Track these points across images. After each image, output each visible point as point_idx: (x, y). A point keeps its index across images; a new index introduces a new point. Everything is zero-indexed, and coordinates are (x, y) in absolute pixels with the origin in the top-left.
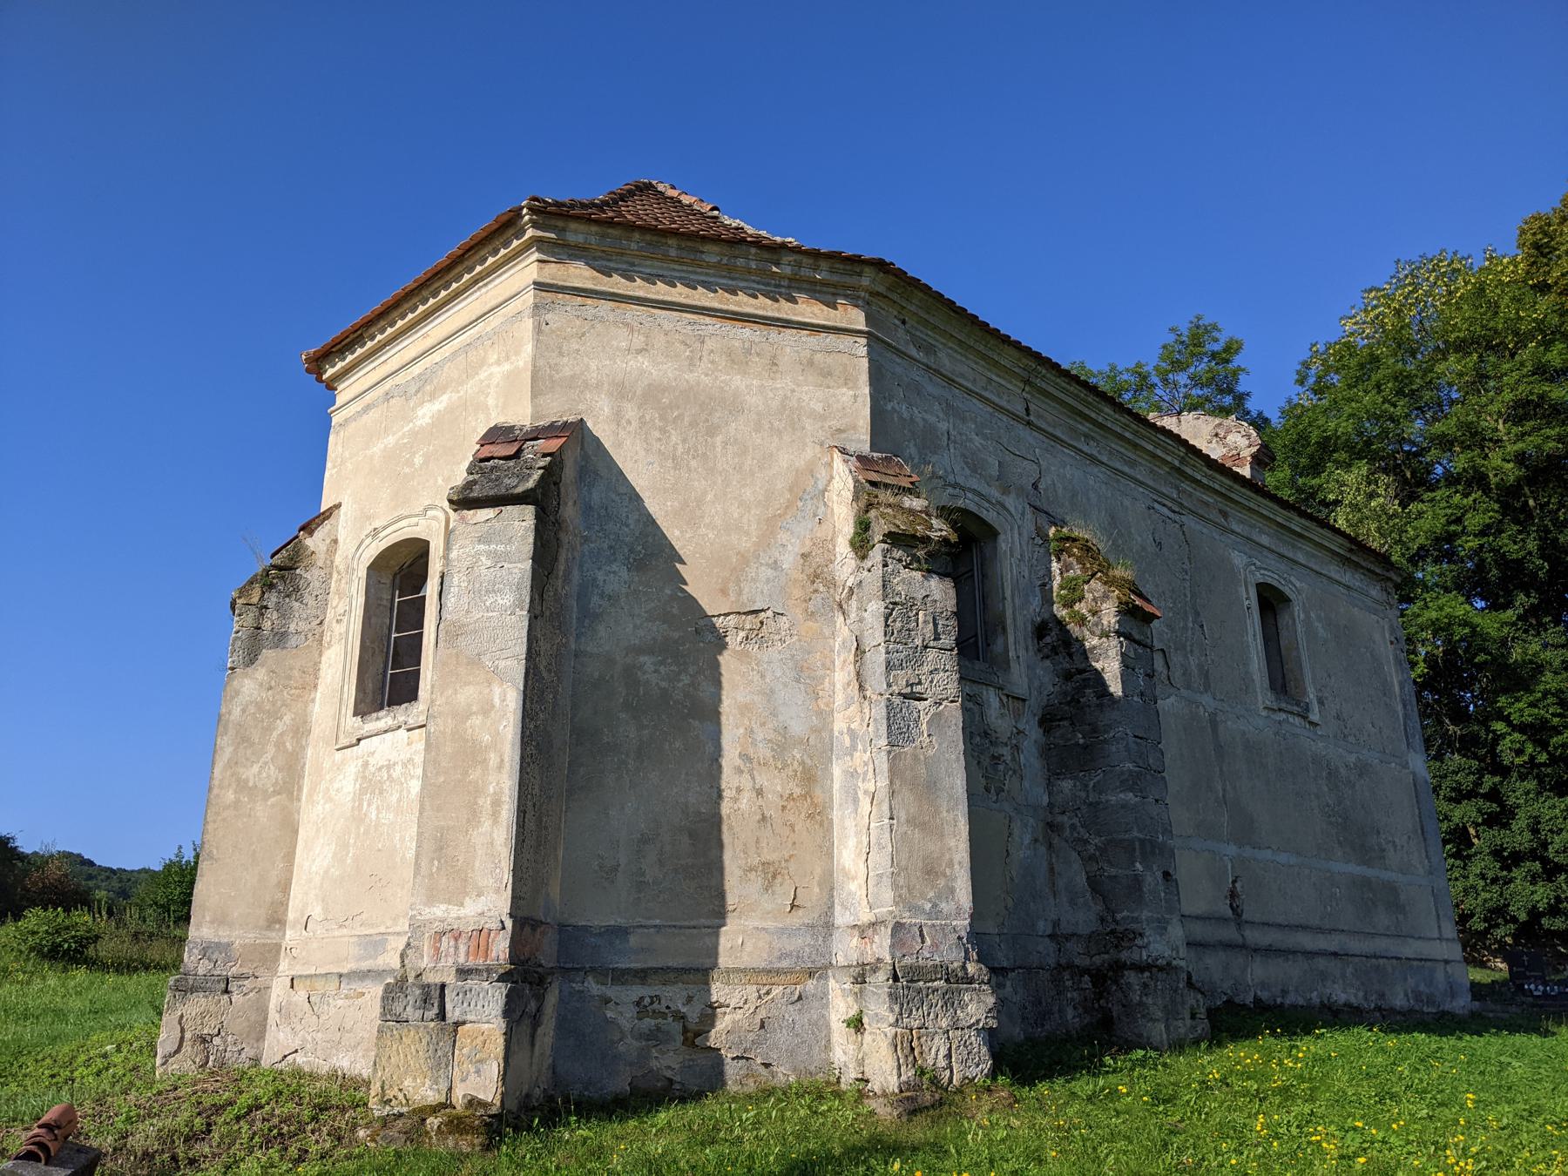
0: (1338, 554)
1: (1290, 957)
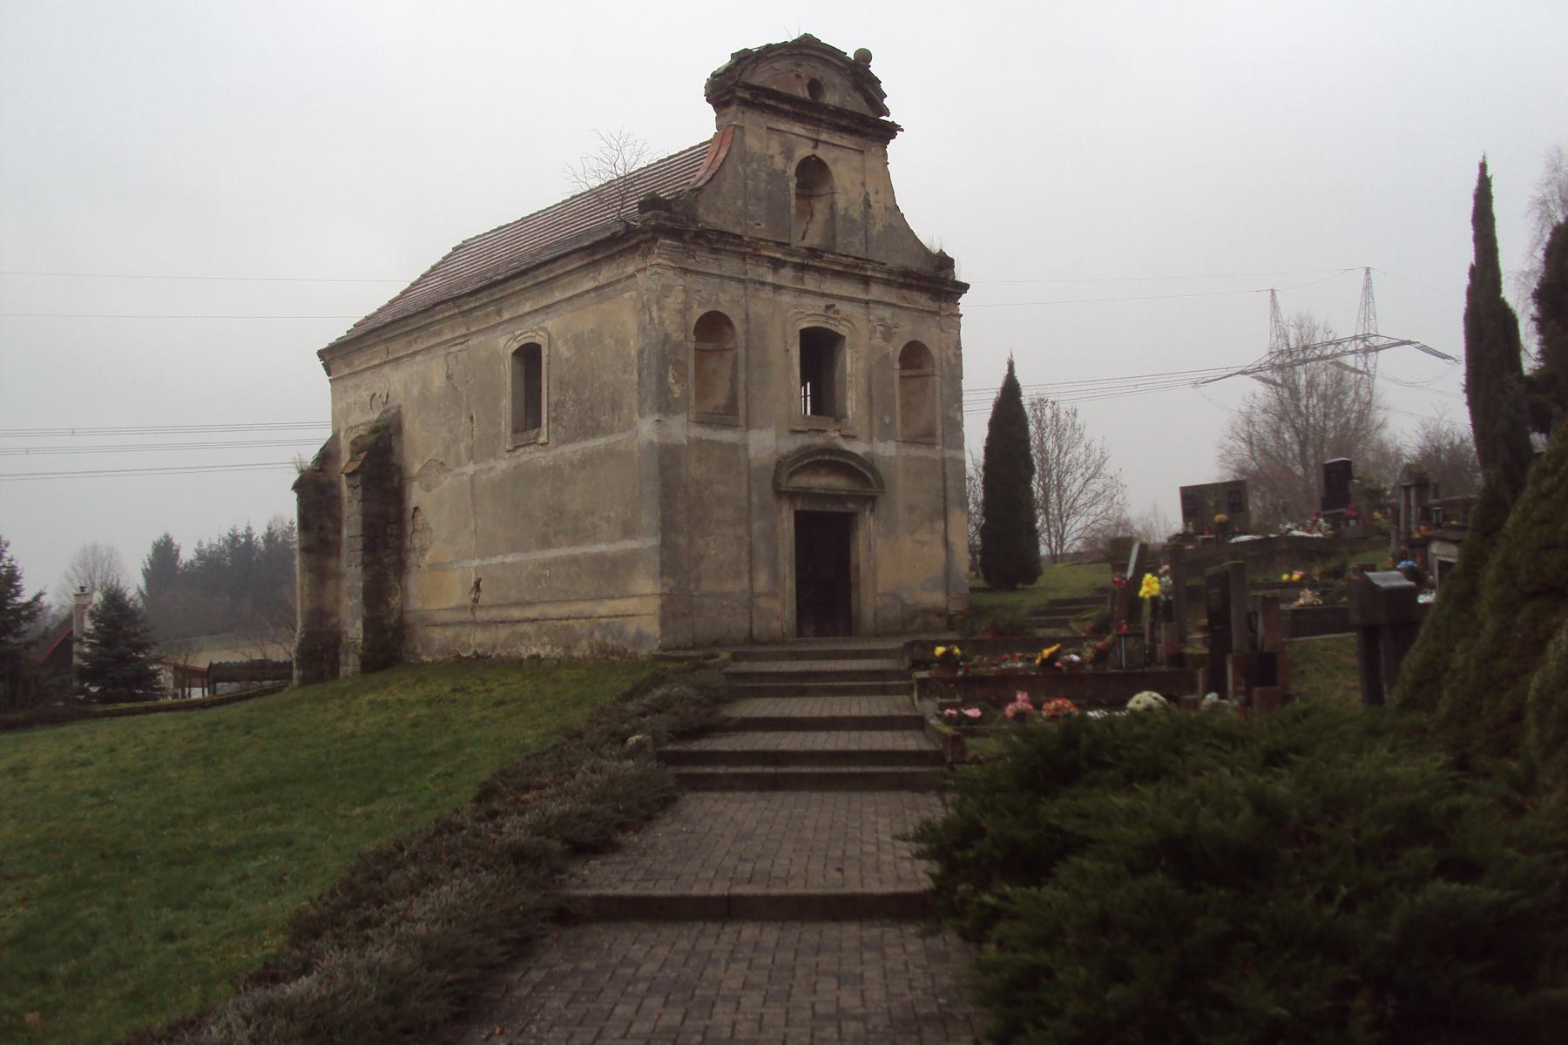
0: (579, 268)
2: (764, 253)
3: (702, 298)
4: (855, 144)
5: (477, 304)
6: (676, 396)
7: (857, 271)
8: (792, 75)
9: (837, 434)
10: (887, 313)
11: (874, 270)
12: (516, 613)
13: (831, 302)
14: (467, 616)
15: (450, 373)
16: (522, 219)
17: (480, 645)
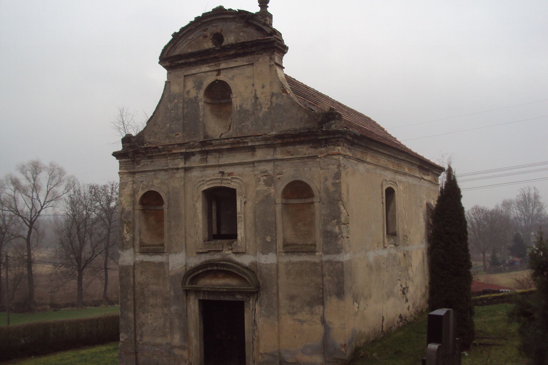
2: (174, 151)
3: (144, 185)
4: (246, 61)
6: (128, 240)
7: (241, 145)
8: (201, 38)
9: (230, 252)
10: (269, 167)
11: (252, 141)
13: (221, 169)
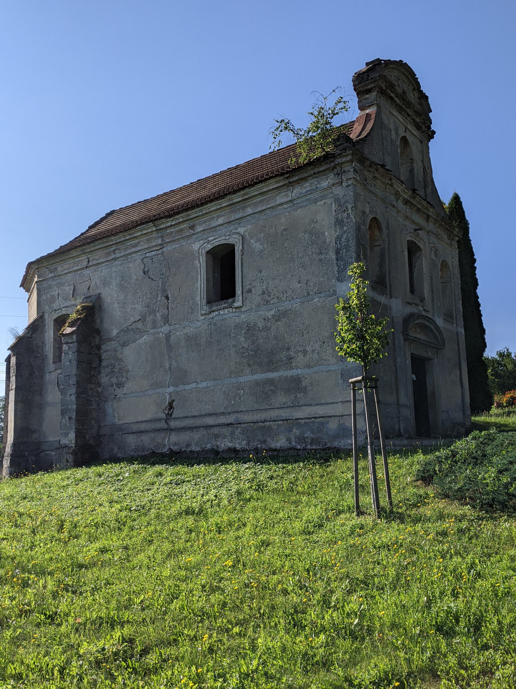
1: (195, 430)
5: (174, 223)
12: (210, 421)
14: (163, 425)
15: (146, 270)
16: (132, 205)
17: (175, 444)
